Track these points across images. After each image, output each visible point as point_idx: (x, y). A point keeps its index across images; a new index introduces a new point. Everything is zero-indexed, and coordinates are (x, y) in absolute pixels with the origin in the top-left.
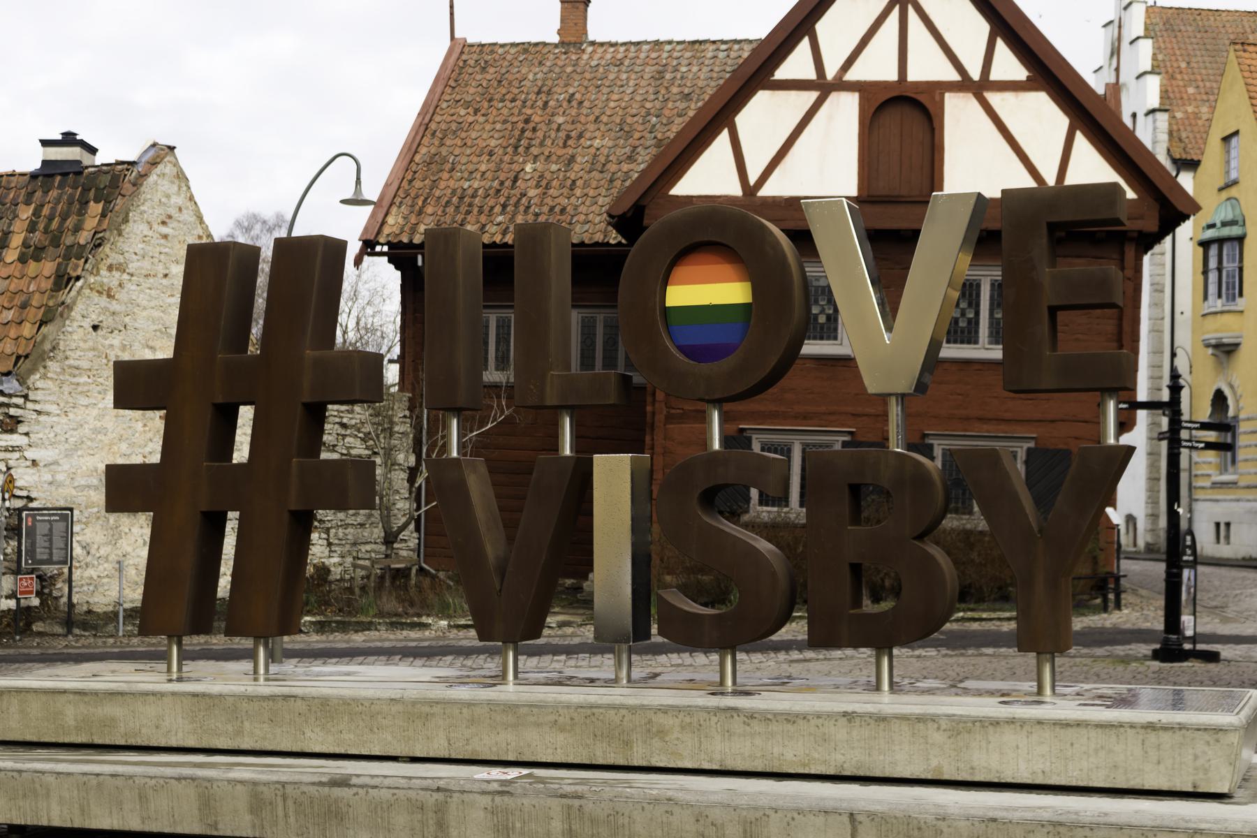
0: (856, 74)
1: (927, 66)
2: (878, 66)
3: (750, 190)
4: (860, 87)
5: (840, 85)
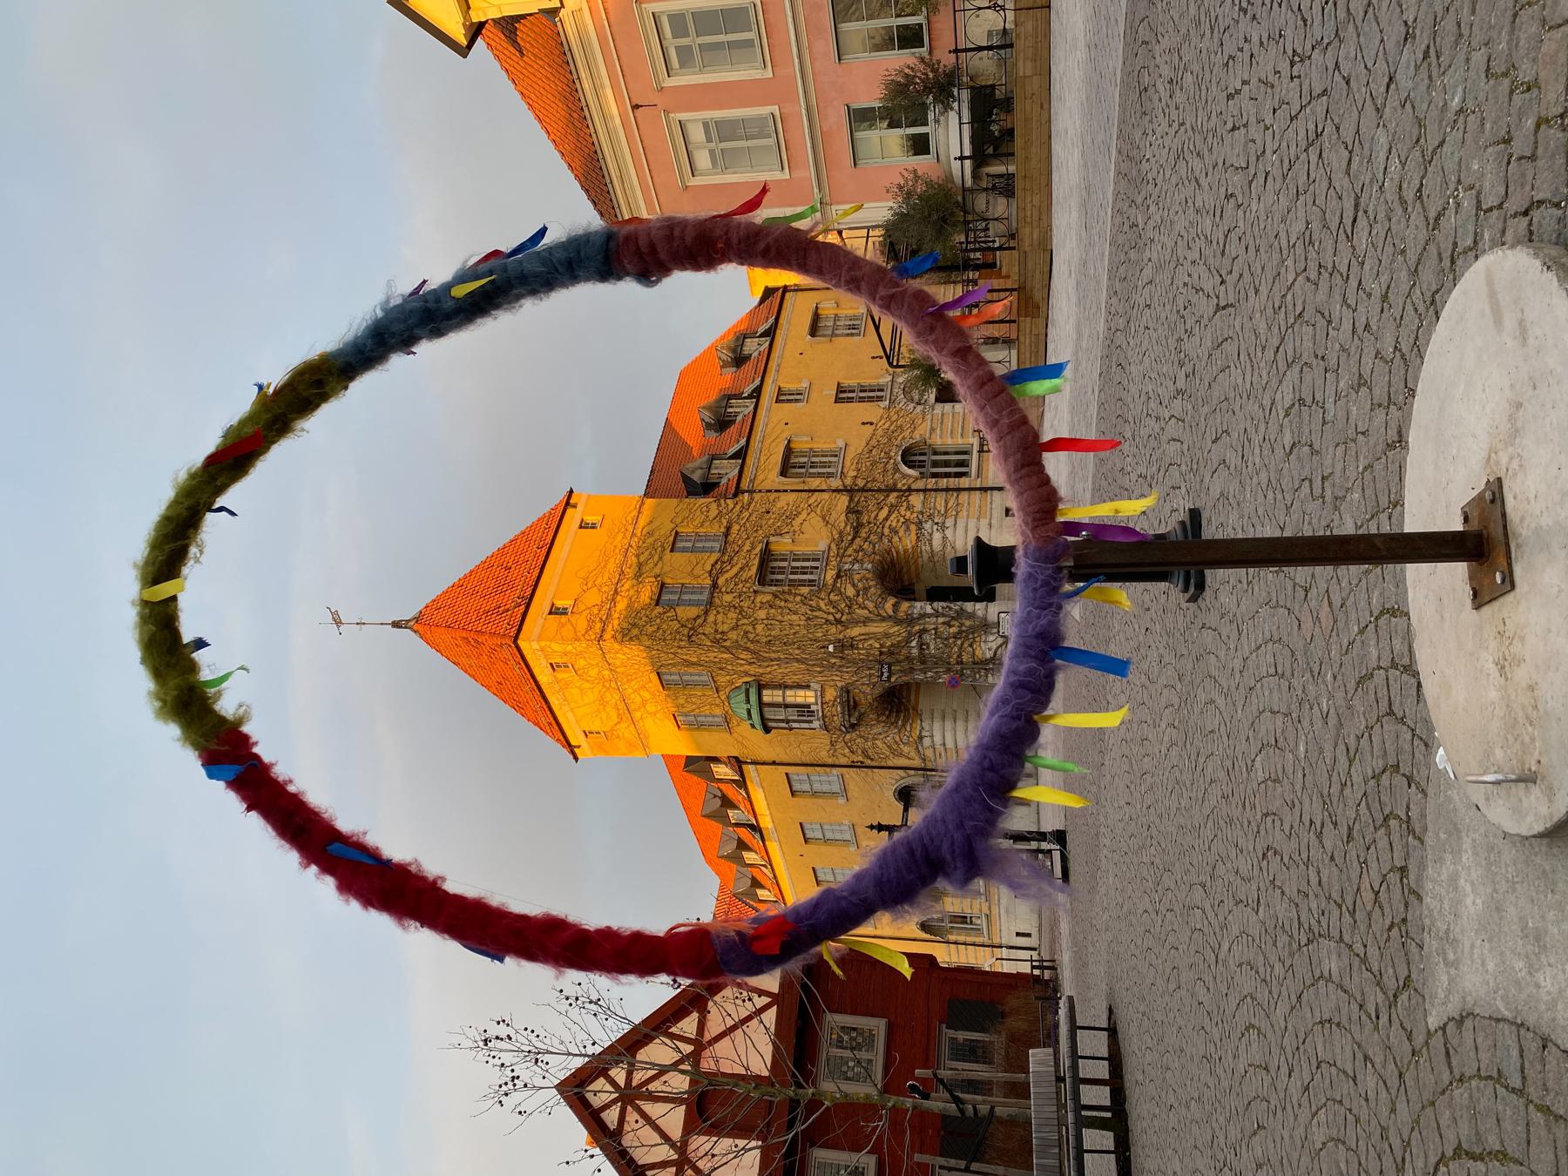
0: (676, 1133)
1: (679, 1083)
2: (673, 1119)
3: (776, 999)
4: (689, 1128)
5: (681, 1148)
